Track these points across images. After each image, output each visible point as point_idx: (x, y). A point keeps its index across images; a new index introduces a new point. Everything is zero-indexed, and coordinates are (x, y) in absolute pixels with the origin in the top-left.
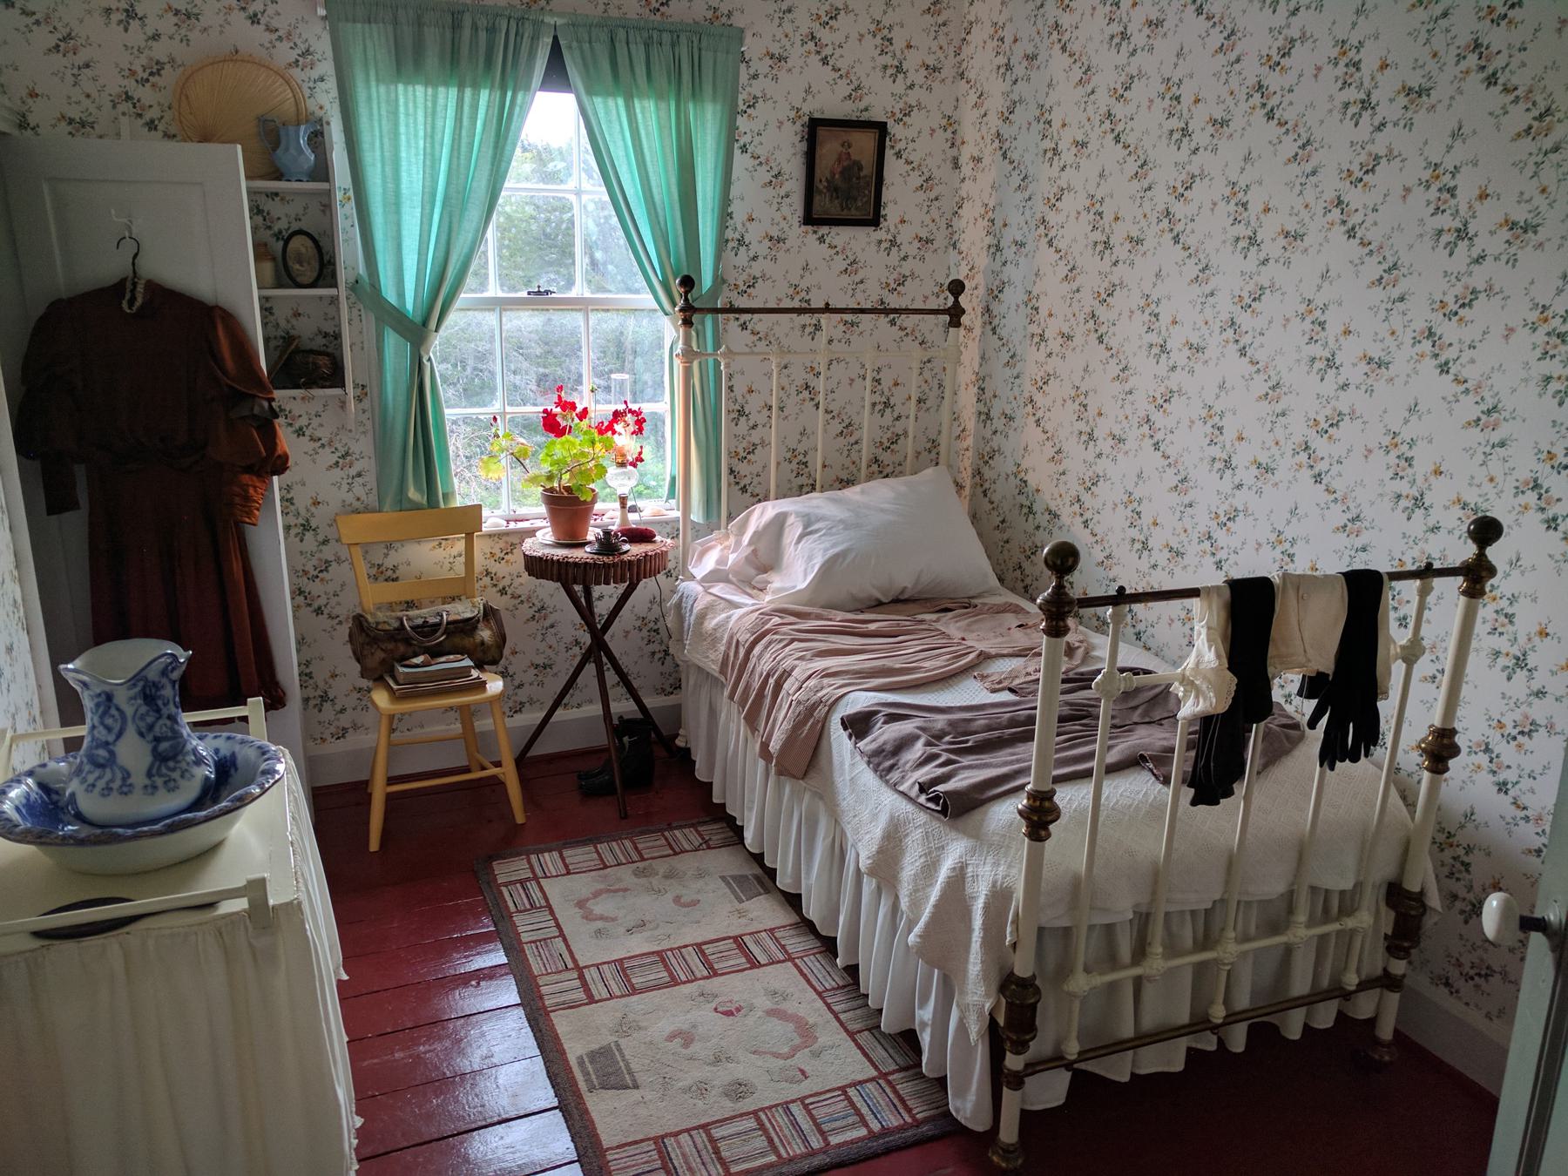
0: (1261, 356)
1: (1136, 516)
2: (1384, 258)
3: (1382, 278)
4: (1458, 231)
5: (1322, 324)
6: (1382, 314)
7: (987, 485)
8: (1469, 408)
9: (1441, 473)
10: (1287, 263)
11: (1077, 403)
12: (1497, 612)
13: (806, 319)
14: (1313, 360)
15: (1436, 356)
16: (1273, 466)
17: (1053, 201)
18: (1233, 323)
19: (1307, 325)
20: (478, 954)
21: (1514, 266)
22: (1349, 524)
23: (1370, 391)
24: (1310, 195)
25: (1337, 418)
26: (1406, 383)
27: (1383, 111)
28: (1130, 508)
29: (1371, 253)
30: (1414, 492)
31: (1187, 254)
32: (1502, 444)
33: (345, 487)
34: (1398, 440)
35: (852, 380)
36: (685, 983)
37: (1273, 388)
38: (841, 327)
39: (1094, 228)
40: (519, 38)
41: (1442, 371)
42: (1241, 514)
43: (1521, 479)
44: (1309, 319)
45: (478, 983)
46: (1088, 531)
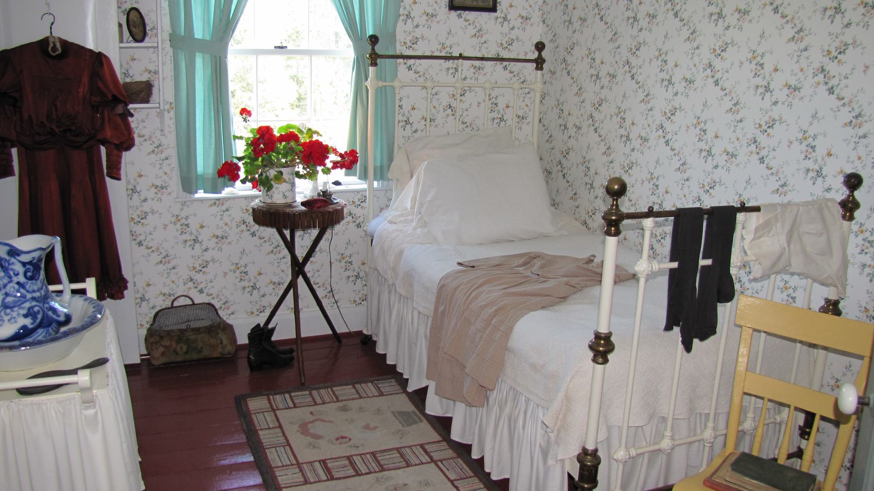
0: (727, 85)
1: (655, 188)
2: (795, 25)
3: (794, 37)
4: (836, 8)
5: (762, 65)
6: (795, 59)
7: (565, 171)
8: (846, 115)
9: (831, 155)
10: (741, 28)
11: (563, 5)
12: (864, 240)
13: (450, 64)
14: (757, 87)
15: (826, 83)
16: (736, 153)
17: (634, 50)
18: (711, 66)
19: (753, 66)
20: (232, 455)
21: (867, 29)
22: (780, 189)
23: (790, 105)
24: (803, 63)
25: (772, 123)
26: (810, 100)
27: (849, 16)
28: (652, 183)
29: (787, 22)
30: (817, 167)
31: (682, 24)
32: (865, 137)
33: (166, 275)
34: (807, 135)
35: (479, 103)
36: (367, 453)
37: (735, 105)
38: (472, 70)
39: (662, 70)
40: (463, 470)
41: (830, 93)
42: (718, 184)
43: (815, 68)
44: (754, 62)
45: (231, 472)
46: (597, 134)
